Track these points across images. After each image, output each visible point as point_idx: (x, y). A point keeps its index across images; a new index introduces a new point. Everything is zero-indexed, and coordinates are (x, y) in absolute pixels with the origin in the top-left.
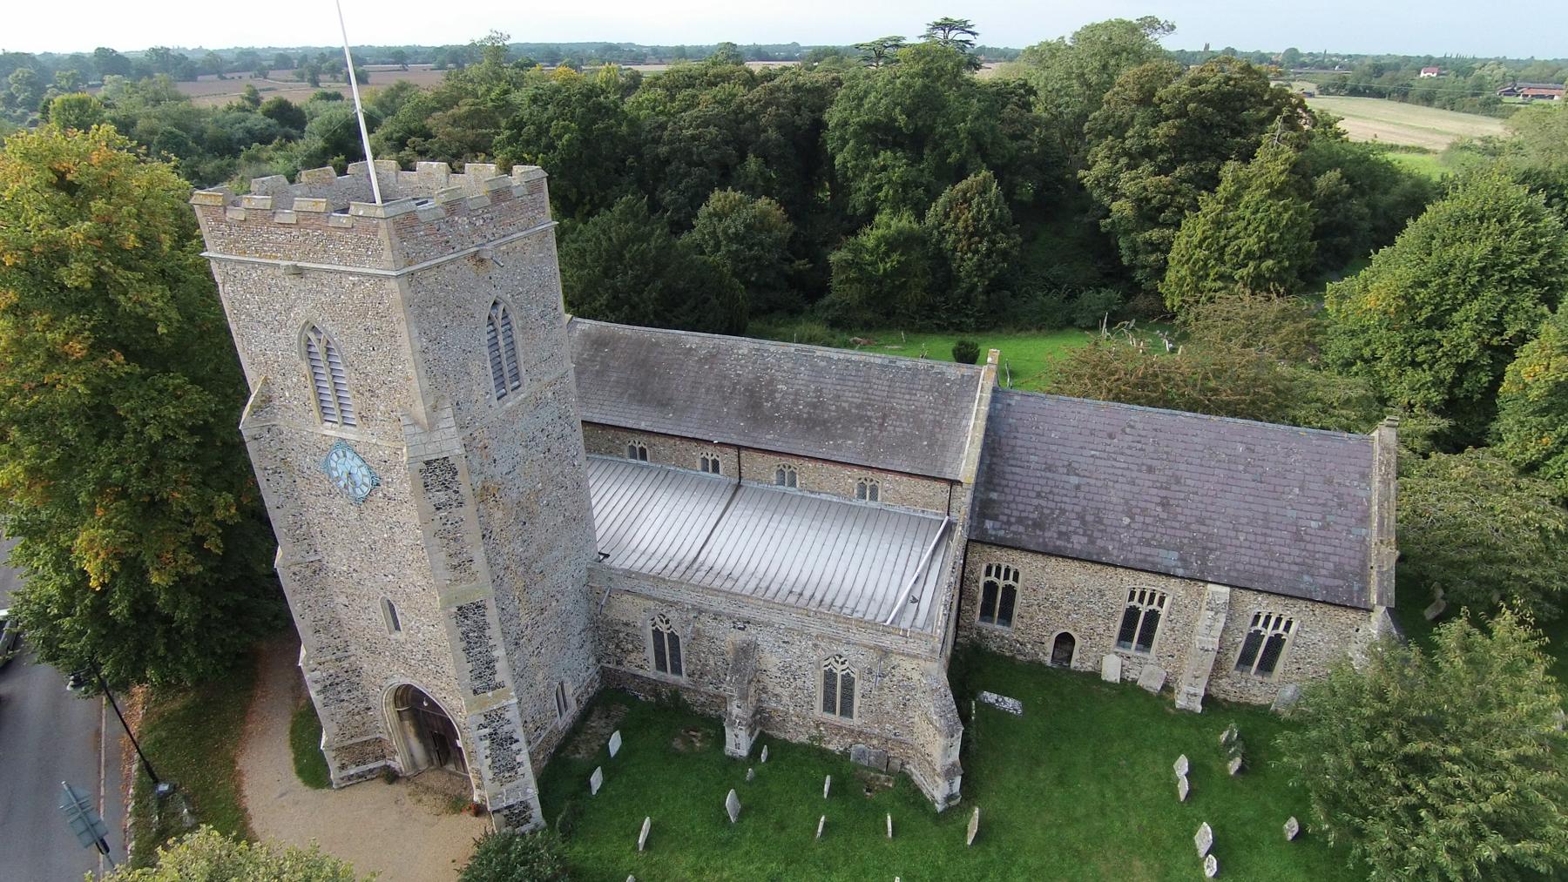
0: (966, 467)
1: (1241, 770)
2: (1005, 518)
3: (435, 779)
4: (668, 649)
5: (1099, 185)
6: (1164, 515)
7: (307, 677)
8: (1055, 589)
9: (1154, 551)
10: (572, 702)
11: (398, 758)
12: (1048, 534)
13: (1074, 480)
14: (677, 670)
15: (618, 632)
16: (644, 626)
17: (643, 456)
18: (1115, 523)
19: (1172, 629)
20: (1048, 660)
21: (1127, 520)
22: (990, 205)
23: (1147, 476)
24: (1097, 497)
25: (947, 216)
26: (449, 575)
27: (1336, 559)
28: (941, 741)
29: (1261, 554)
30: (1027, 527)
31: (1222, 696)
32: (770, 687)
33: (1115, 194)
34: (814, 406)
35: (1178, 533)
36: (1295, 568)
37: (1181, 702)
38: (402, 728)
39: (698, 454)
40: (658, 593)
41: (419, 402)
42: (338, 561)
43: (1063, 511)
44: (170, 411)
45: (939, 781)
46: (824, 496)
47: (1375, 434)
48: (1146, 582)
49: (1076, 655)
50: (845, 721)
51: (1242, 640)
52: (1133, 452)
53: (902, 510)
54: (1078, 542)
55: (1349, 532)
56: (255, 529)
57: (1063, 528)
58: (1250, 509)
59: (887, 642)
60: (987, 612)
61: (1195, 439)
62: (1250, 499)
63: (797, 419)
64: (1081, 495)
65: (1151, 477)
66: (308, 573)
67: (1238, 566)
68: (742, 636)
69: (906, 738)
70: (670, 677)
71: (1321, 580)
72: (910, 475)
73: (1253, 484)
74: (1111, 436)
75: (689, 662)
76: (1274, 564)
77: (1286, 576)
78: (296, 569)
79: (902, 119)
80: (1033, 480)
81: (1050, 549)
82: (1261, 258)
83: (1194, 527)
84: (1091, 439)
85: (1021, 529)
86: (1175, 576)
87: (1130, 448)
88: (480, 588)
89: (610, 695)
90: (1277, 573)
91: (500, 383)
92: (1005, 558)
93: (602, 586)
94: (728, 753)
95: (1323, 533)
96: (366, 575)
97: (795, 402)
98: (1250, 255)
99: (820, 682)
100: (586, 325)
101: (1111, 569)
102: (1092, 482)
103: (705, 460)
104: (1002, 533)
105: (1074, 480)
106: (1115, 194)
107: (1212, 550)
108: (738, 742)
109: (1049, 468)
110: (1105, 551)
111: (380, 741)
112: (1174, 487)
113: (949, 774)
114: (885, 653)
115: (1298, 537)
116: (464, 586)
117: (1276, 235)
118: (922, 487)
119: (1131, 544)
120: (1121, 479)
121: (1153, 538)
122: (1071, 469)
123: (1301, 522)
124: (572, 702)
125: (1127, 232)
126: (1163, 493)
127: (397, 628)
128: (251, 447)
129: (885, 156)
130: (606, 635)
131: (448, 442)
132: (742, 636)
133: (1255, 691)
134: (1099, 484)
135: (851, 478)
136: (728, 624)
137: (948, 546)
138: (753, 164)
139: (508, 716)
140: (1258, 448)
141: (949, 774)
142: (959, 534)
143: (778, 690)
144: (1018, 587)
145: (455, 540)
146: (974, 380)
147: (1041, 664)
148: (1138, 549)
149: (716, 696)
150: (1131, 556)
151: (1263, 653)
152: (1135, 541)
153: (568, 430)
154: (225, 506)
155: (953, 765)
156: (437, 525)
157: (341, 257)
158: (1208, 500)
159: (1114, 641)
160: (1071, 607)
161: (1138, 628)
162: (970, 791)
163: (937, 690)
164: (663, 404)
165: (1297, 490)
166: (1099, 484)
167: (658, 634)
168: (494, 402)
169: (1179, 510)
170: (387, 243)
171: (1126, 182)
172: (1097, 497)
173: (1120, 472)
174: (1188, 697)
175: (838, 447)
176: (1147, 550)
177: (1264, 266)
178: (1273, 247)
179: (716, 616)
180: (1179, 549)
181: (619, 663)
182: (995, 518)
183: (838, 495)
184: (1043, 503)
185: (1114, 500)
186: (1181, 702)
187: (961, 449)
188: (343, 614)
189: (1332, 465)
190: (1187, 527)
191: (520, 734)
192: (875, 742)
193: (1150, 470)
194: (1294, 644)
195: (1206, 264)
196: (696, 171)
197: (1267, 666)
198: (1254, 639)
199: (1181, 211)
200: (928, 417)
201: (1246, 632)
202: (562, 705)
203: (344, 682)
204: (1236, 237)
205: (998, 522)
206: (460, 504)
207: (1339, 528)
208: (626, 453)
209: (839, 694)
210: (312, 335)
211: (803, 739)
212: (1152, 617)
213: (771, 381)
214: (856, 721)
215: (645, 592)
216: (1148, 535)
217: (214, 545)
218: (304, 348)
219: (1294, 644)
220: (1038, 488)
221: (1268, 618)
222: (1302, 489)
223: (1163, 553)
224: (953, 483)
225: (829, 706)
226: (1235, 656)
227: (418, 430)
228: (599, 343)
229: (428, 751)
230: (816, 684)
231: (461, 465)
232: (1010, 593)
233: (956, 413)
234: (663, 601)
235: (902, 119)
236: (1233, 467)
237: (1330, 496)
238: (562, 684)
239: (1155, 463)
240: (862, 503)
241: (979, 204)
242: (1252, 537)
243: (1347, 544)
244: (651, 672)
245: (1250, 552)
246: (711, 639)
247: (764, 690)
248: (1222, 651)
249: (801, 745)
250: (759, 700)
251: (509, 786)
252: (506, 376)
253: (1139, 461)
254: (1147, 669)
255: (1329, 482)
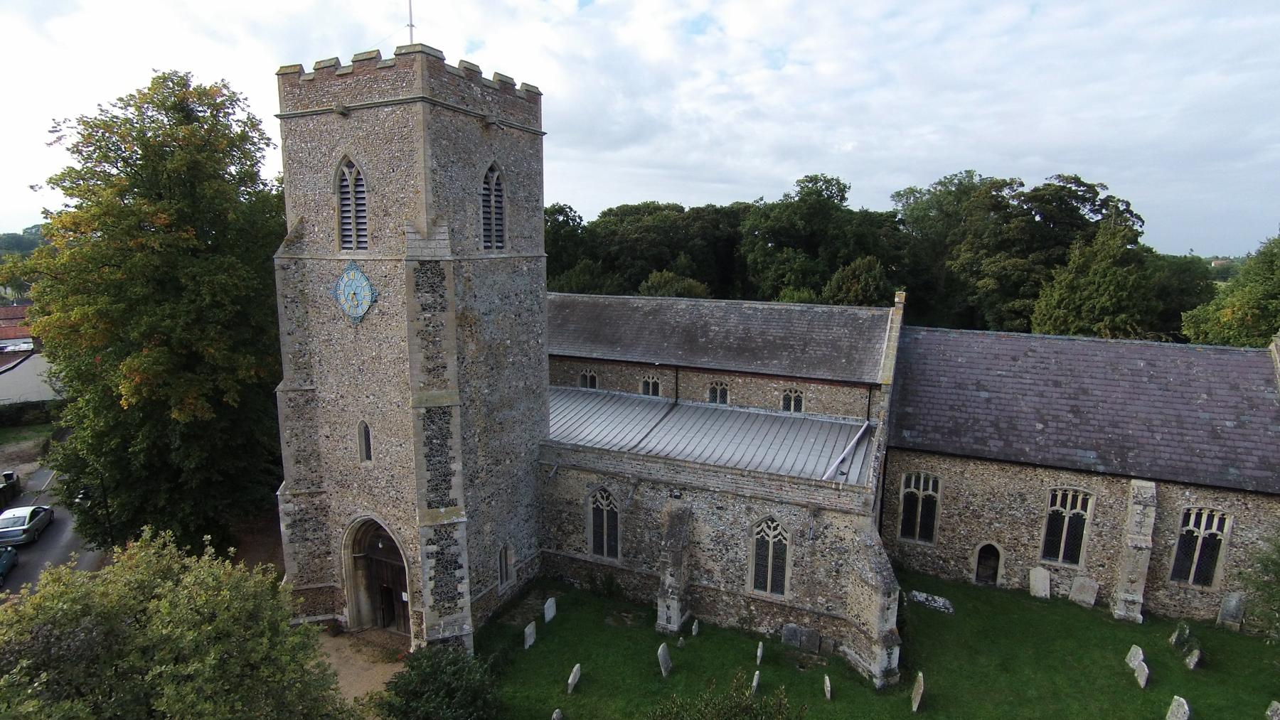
0: (884, 372)
1: (1200, 663)
2: (921, 428)
3: (377, 636)
4: (606, 526)
5: (964, 270)
6: (1077, 421)
7: (281, 507)
8: (975, 496)
9: (1072, 451)
10: (513, 571)
11: (346, 611)
12: (964, 440)
13: (984, 395)
14: (613, 552)
15: (561, 512)
16: (586, 504)
17: (593, 385)
18: (1029, 428)
19: (1100, 535)
20: (972, 576)
21: (1040, 426)
22: (875, 279)
23: (1053, 389)
24: (1008, 408)
25: (840, 288)
26: (424, 377)
27: (1260, 453)
28: (878, 599)
29: (1180, 451)
30: (943, 434)
31: (1162, 612)
32: (702, 562)
33: (979, 275)
34: (742, 339)
35: (1093, 435)
36: (1220, 462)
37: (1119, 611)
38: (355, 577)
39: (640, 378)
40: (601, 465)
41: (423, 212)
42: (327, 393)
43: (977, 421)
44: (222, 278)
45: (877, 649)
46: (752, 410)
47: (1272, 347)
48: (1067, 481)
49: (1001, 571)
50: (777, 598)
51: (1174, 541)
52: (1038, 370)
53: (825, 419)
54: (995, 446)
55: (1267, 430)
56: (262, 394)
57: (979, 434)
58: (1161, 413)
59: (820, 498)
60: (908, 531)
61: (1096, 359)
62: (1161, 405)
63: (729, 349)
64: (993, 407)
65: (1058, 390)
66: (302, 401)
67: (1160, 462)
68: (677, 504)
69: (839, 612)
70: (606, 559)
71: (1248, 472)
72: (831, 382)
73: (1160, 393)
74: (1014, 359)
75: (625, 540)
76: (1197, 459)
77: (1211, 469)
78: (292, 395)
79: (800, 224)
80: (945, 396)
81: (967, 452)
82: (1115, 313)
83: (1107, 429)
84: (996, 362)
85: (938, 436)
86: (1098, 473)
87: (1034, 367)
88: (447, 396)
89: (548, 576)
90: (1203, 467)
91: (488, 238)
92: (925, 465)
93: (555, 460)
94: (658, 629)
95: (1240, 431)
96: (350, 399)
97: (726, 338)
98: (1104, 311)
99: (752, 551)
100: (553, 296)
101: (1030, 471)
102: (1002, 395)
103: (646, 384)
104: (920, 440)
105: (984, 395)
106: (979, 275)
107: (1130, 449)
108: (669, 614)
109: (960, 386)
110: (1022, 451)
111: (333, 590)
112: (1081, 397)
113: (887, 641)
114: (817, 511)
115: (1215, 435)
116: (435, 392)
117: (1125, 294)
118: (844, 394)
119: (1048, 446)
120: (1029, 393)
121: (1069, 440)
122: (979, 386)
123: (1215, 423)
124: (513, 571)
125: (992, 305)
126: (1073, 402)
127: (369, 458)
128: (279, 275)
129: (788, 252)
130: (550, 514)
131: (440, 249)
132: (677, 504)
133: (1196, 603)
134: (1008, 397)
135: (776, 391)
136: (665, 493)
137: (870, 441)
138: (683, 259)
139: (456, 535)
140: (1158, 363)
141: (887, 641)
142: (879, 437)
143: (711, 565)
144: (939, 496)
145: (434, 343)
146: (884, 319)
147: (966, 582)
148: (1055, 450)
149: (649, 577)
150: (1047, 456)
151: (1196, 557)
152: (1051, 443)
153: (536, 308)
154: (247, 366)
155: (891, 632)
156: (420, 325)
157: (382, 94)
158: (1118, 407)
159: (1039, 552)
160: (992, 515)
161: (1063, 539)
162: (907, 667)
163: (871, 547)
164: (612, 342)
165: (1205, 396)
166: (1008, 397)
167: (598, 512)
168: (481, 247)
169: (1090, 416)
170: (419, 72)
171: (988, 265)
172: (1008, 408)
173: (1027, 387)
174: (1127, 602)
175: (766, 365)
176: (1064, 451)
177: (1118, 319)
178: (1124, 304)
179: (655, 484)
180: (1096, 448)
181: (559, 547)
182: (911, 428)
183: (765, 408)
184: (957, 414)
185: (1025, 409)
186: (1119, 611)
187: (877, 363)
188: (324, 447)
189: (1235, 374)
190: (1101, 430)
191: (464, 560)
192: (807, 620)
193: (1057, 384)
194: (1231, 544)
195: (1065, 321)
196: (639, 263)
197: (1205, 577)
198: (1187, 541)
199: (1038, 284)
200: (845, 344)
201: (1178, 532)
202: (505, 576)
203: (313, 519)
204: (1089, 298)
205: (914, 430)
206: (443, 309)
207: (1254, 426)
208: (579, 381)
209: (770, 565)
210: (346, 170)
211: (733, 621)
212: (1078, 522)
213: (706, 324)
214: (788, 596)
215: (591, 465)
216: (1063, 438)
217: (230, 399)
218: (338, 183)
219: (1231, 544)
220: (951, 403)
221: (1199, 516)
222: (1209, 394)
223: (1080, 452)
224: (873, 387)
225: (760, 583)
226: (1170, 562)
227: (418, 237)
228: (561, 306)
229: (374, 609)
230: (745, 552)
231: (449, 271)
232: (930, 503)
233: (869, 340)
234: (604, 474)
235: (800, 224)
236: (1137, 379)
237: (1239, 399)
238: (506, 549)
239: (1060, 379)
240: (787, 414)
241: (866, 279)
242: (1168, 437)
243: (1267, 440)
244: (588, 555)
245: (1168, 449)
246: (648, 511)
247: (697, 566)
248: (1156, 556)
249: (732, 628)
250: (691, 579)
251: (447, 618)
252: (493, 234)
253: (1045, 378)
254: (1078, 581)
255: (1235, 387)
